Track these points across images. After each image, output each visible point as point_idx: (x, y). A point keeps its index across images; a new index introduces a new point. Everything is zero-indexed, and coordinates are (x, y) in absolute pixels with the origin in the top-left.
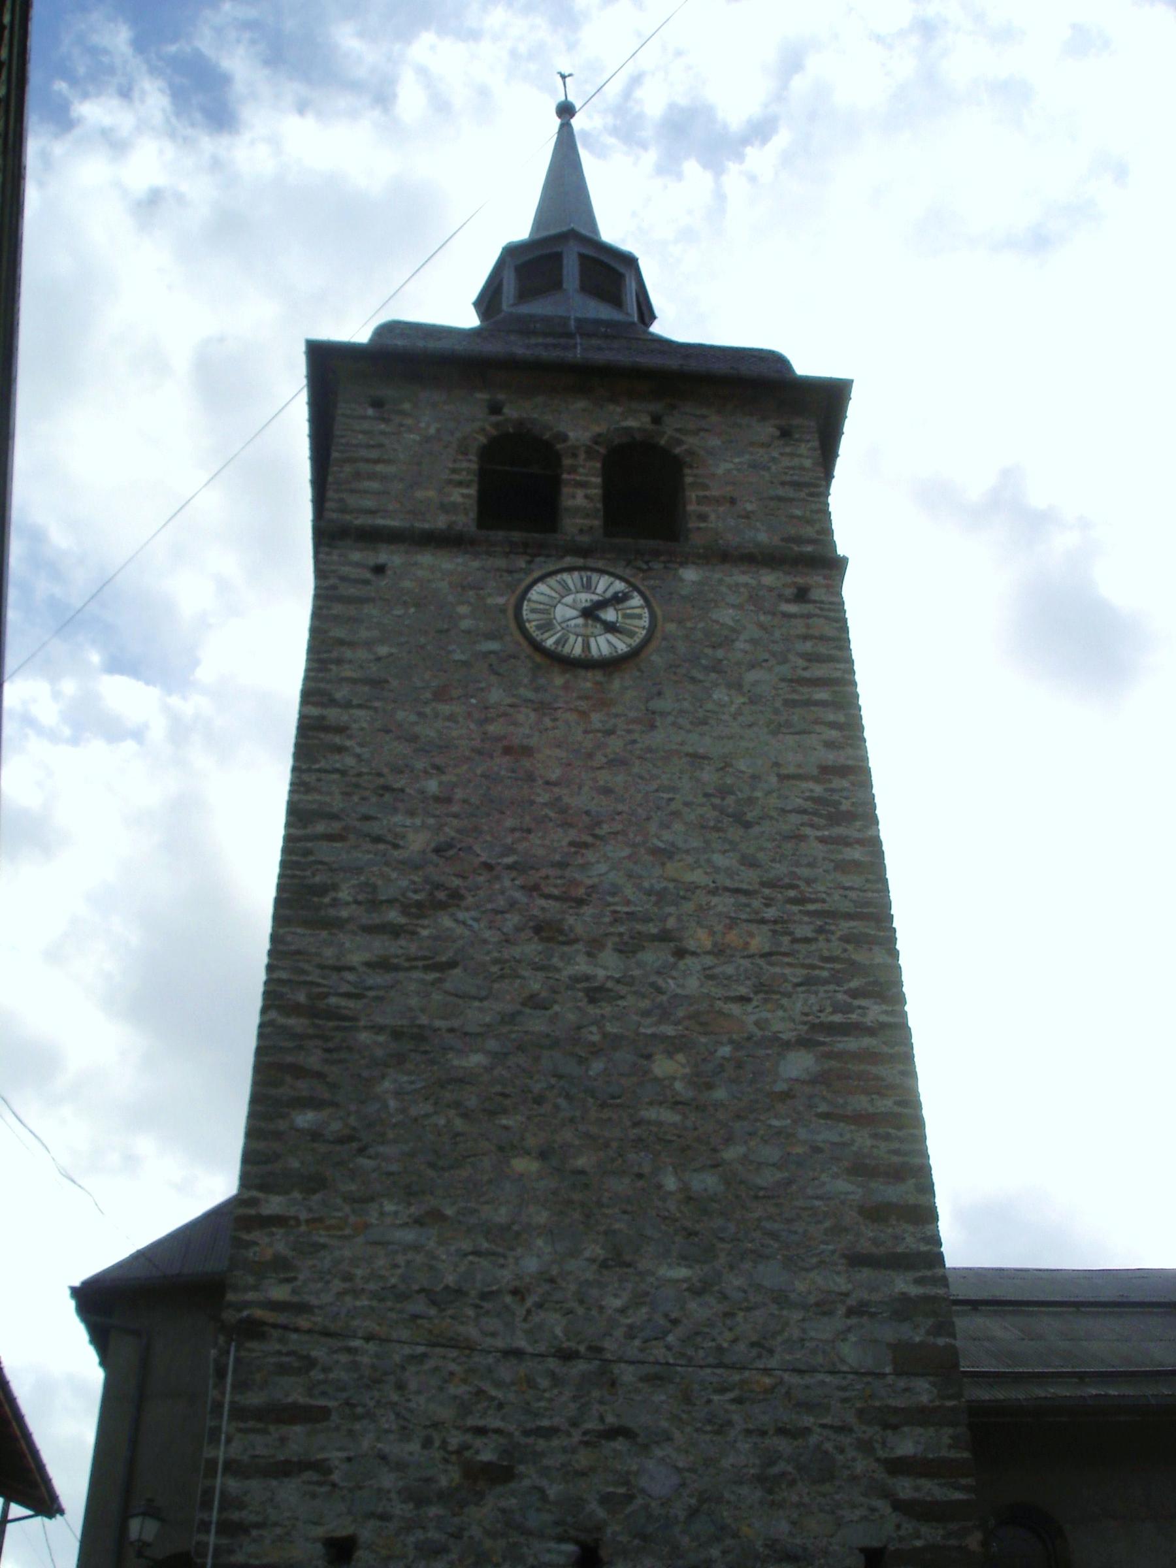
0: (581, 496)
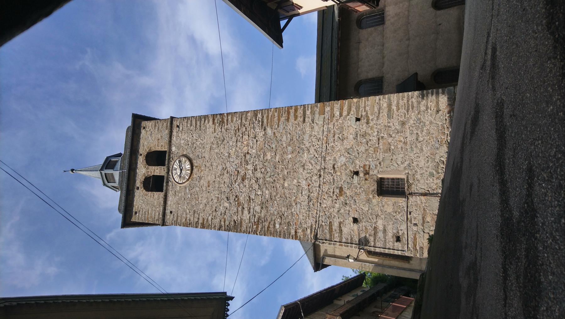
0: (158, 171)
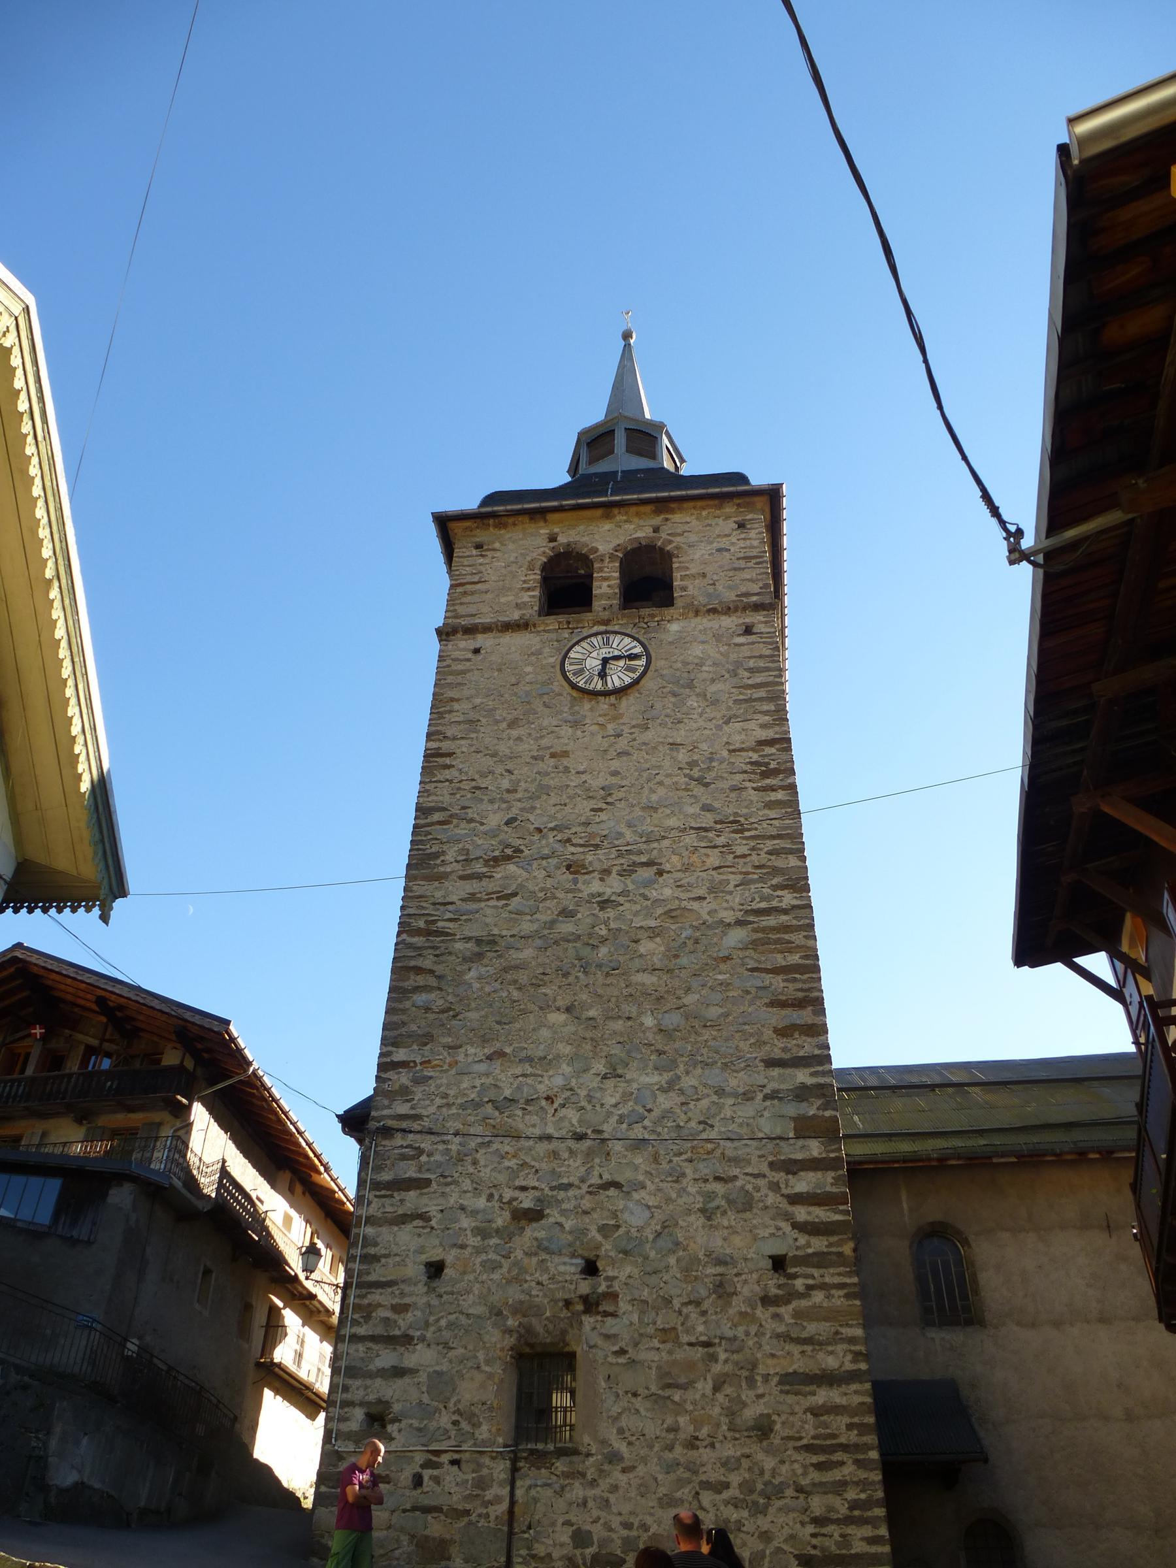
0: (606, 585)
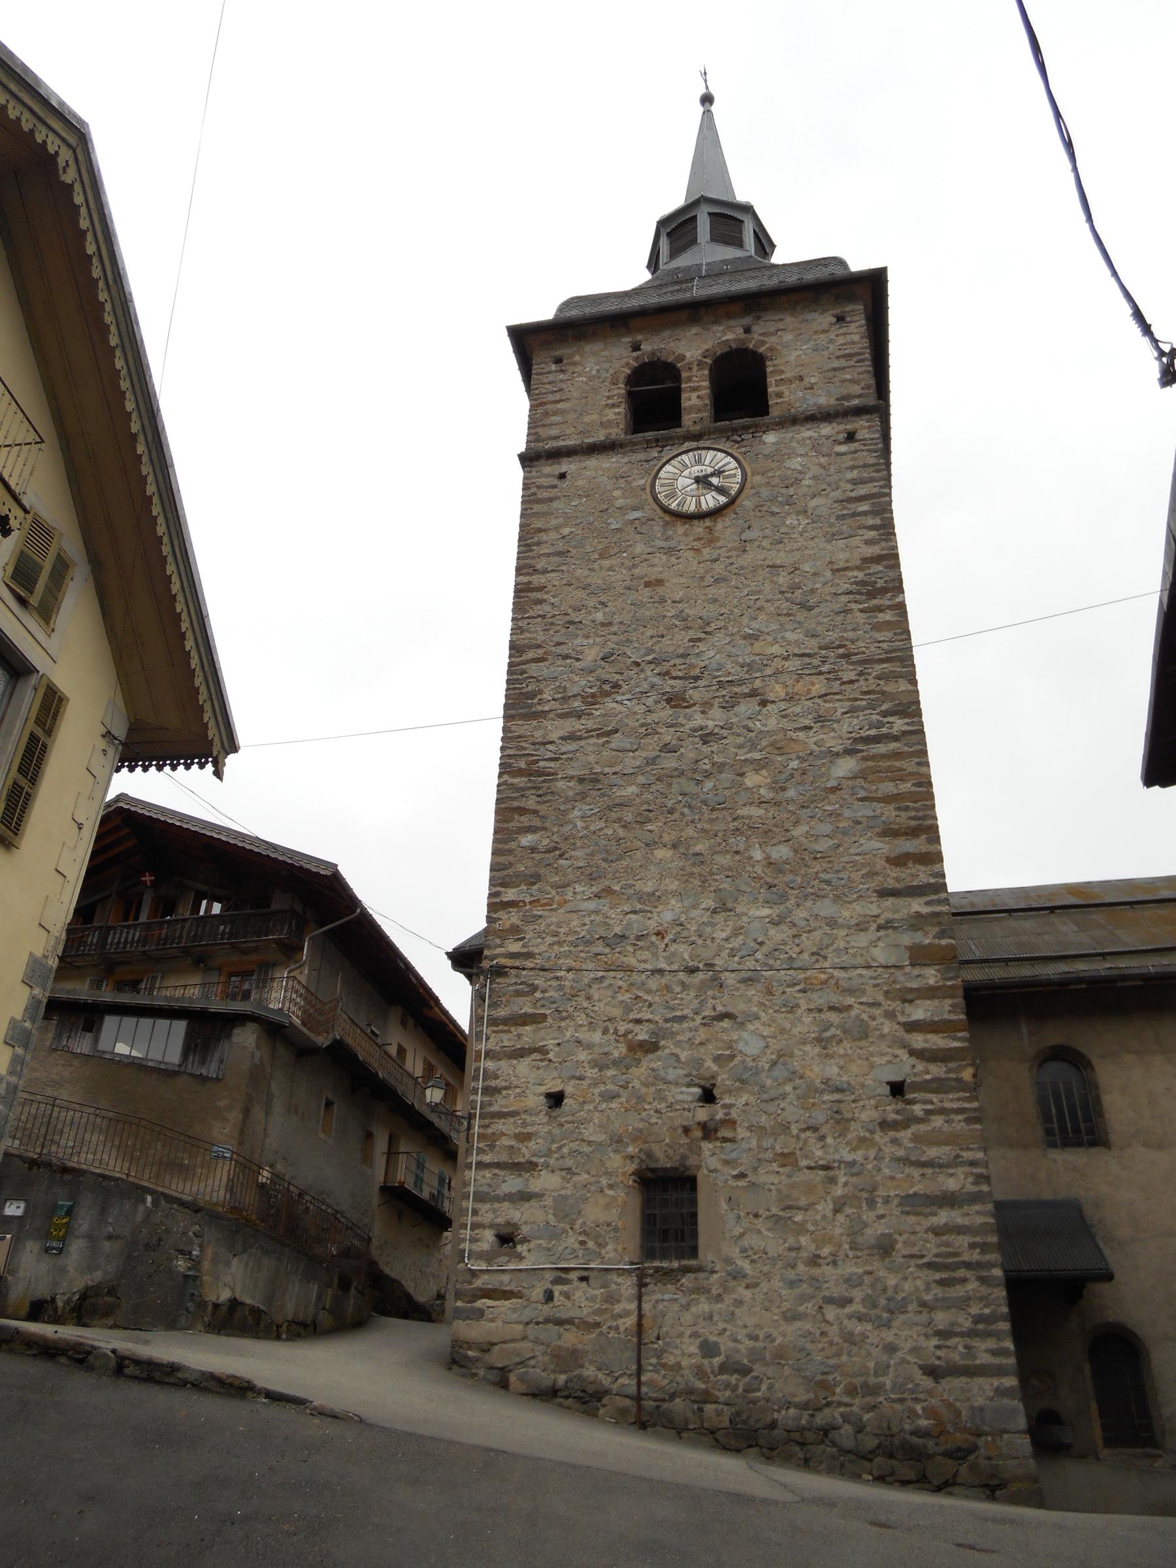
0: (696, 397)
